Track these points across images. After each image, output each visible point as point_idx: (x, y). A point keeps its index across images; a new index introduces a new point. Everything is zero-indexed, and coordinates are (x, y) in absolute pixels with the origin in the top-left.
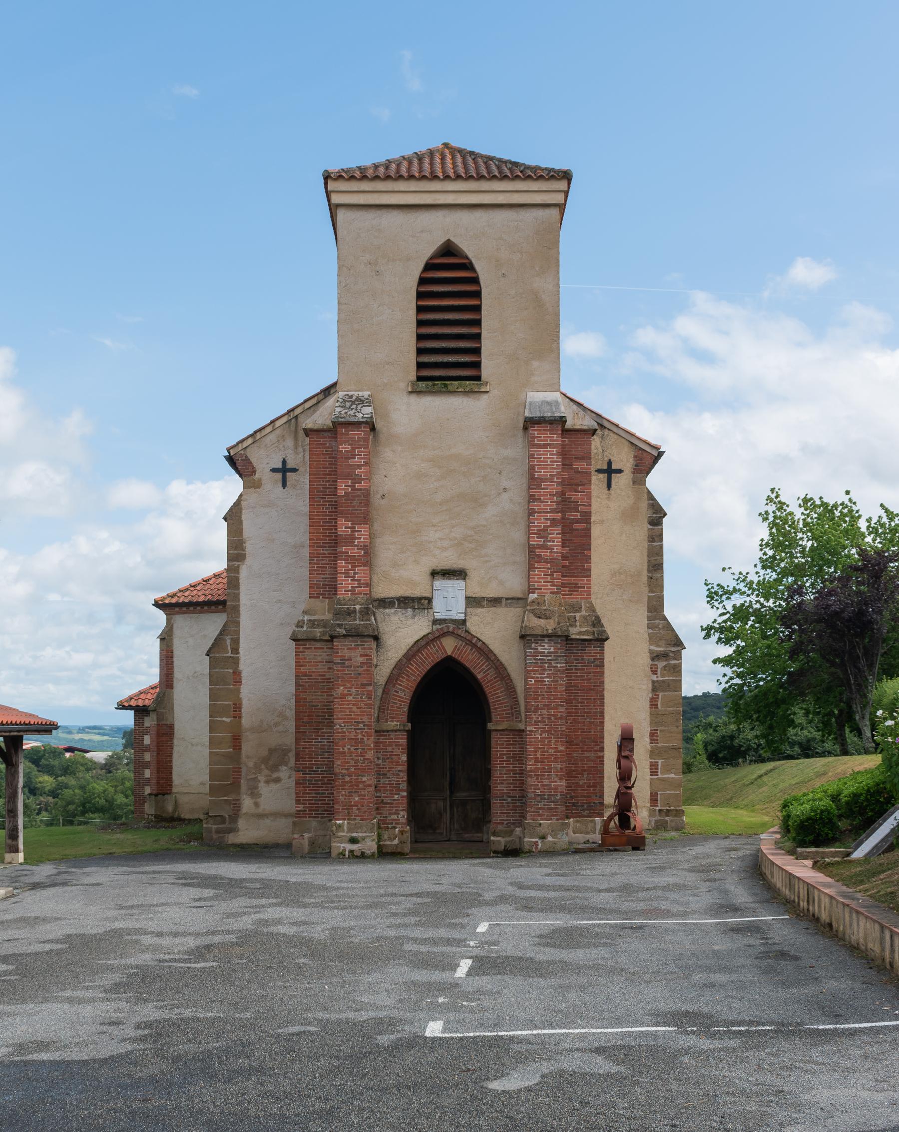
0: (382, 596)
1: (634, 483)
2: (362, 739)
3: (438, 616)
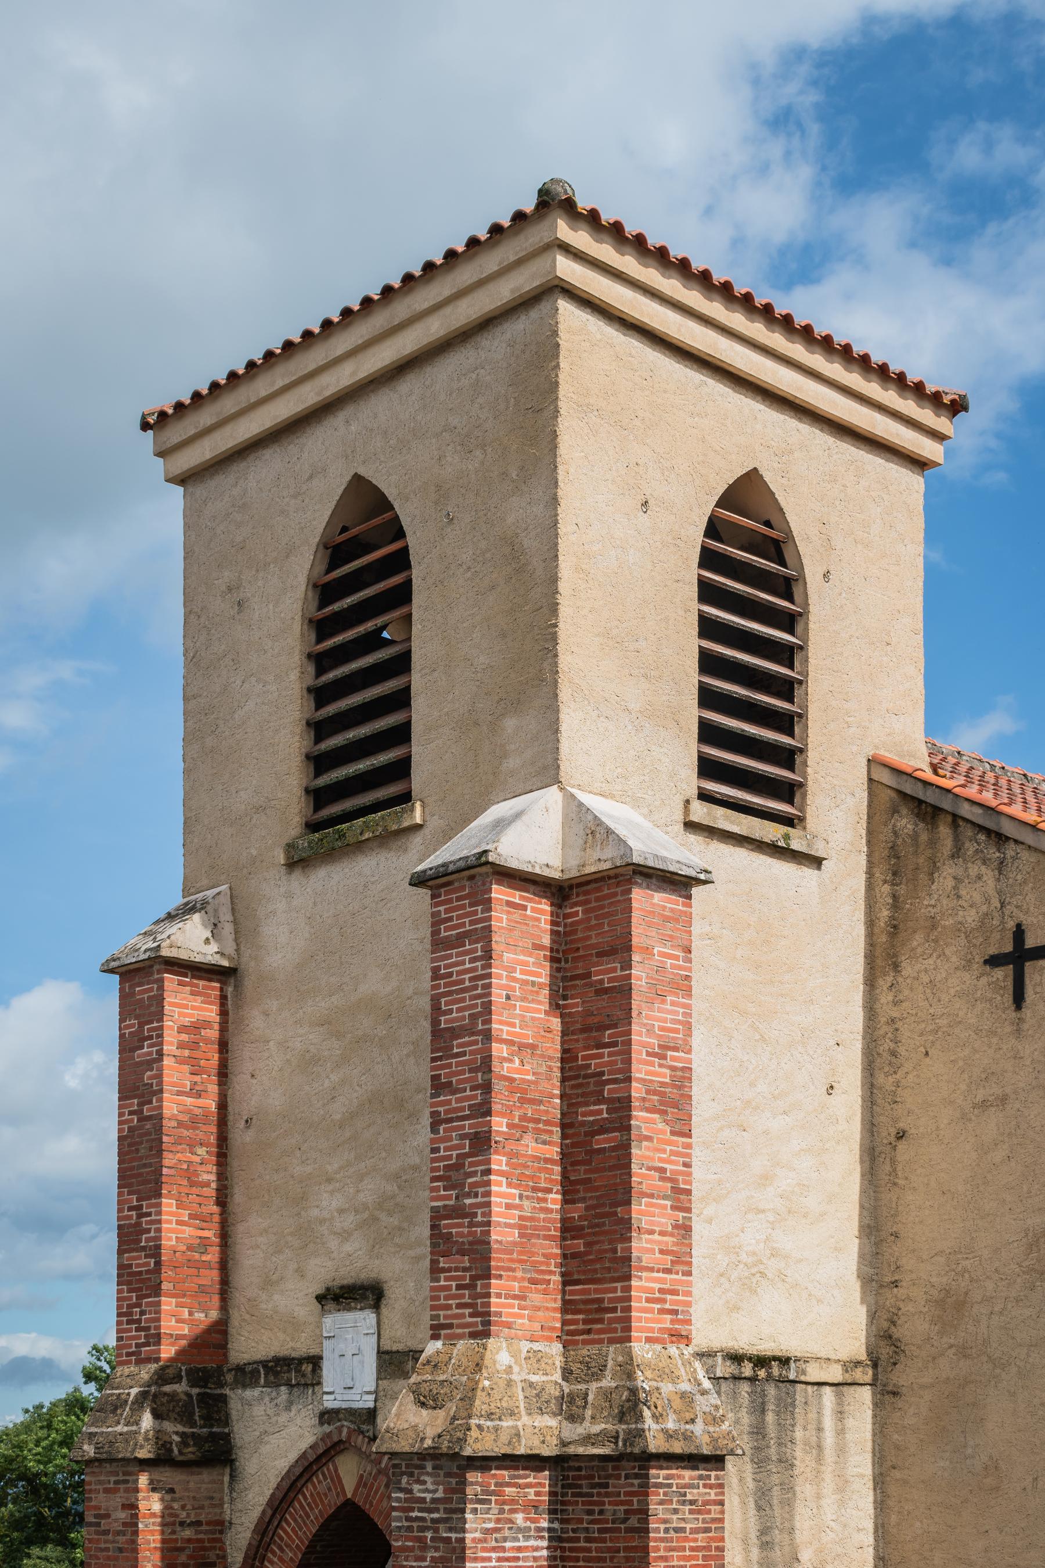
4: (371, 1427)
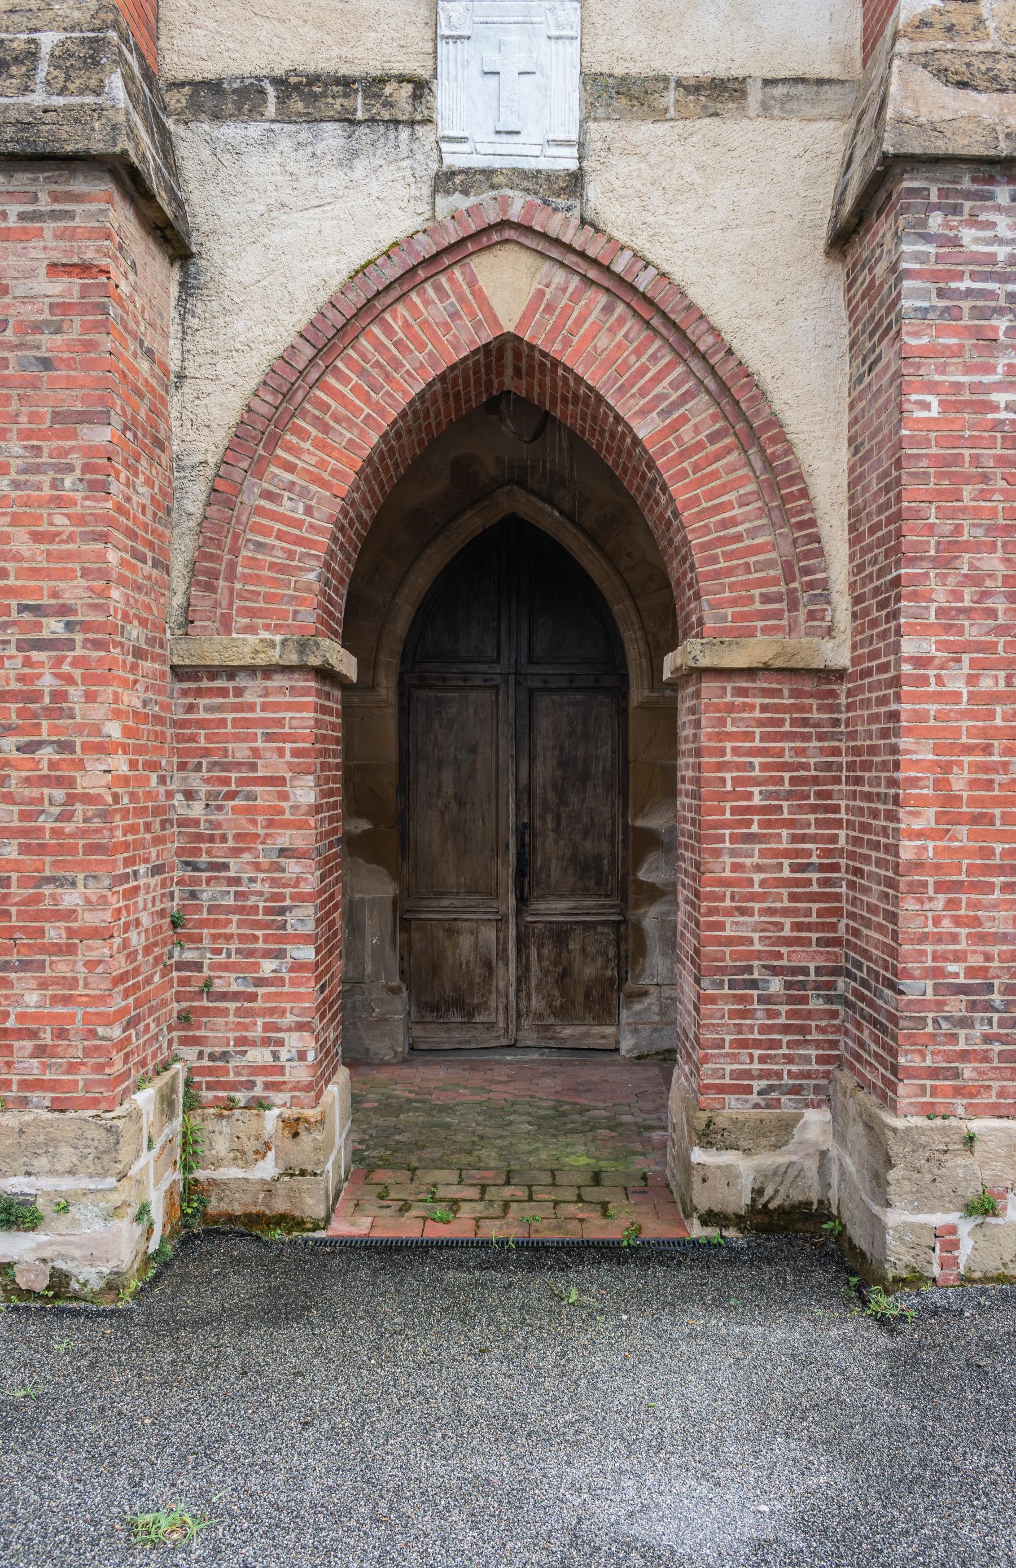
0: (210, 70)
2: (59, 696)
3: (457, 158)
4: (577, 203)
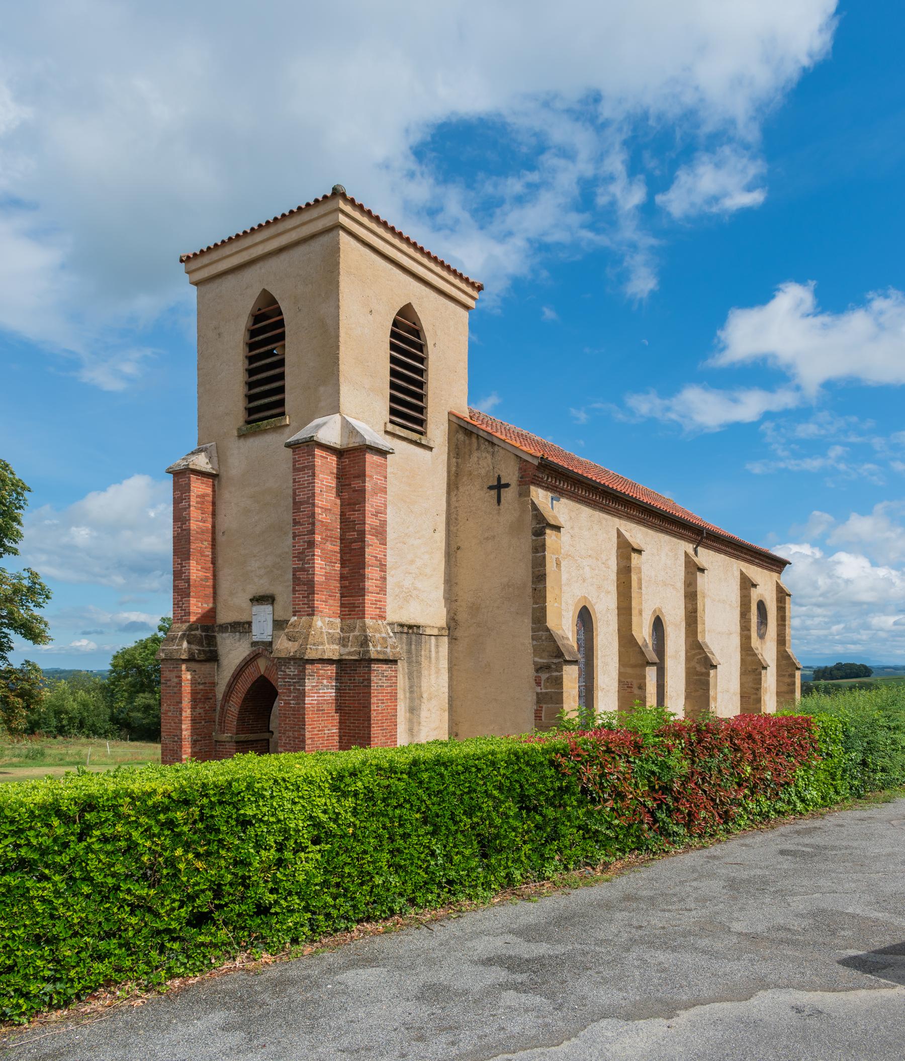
1: (520, 495)
